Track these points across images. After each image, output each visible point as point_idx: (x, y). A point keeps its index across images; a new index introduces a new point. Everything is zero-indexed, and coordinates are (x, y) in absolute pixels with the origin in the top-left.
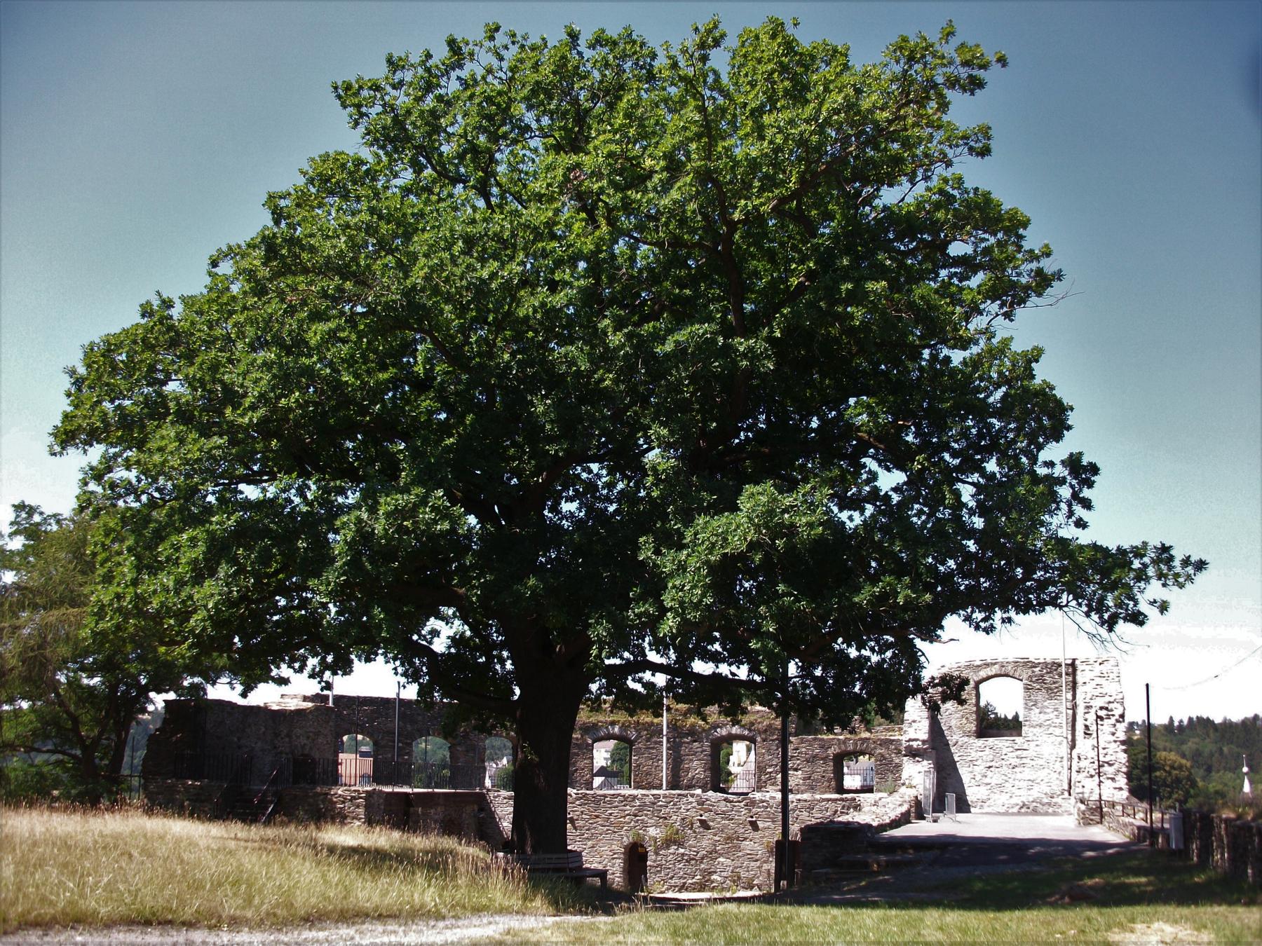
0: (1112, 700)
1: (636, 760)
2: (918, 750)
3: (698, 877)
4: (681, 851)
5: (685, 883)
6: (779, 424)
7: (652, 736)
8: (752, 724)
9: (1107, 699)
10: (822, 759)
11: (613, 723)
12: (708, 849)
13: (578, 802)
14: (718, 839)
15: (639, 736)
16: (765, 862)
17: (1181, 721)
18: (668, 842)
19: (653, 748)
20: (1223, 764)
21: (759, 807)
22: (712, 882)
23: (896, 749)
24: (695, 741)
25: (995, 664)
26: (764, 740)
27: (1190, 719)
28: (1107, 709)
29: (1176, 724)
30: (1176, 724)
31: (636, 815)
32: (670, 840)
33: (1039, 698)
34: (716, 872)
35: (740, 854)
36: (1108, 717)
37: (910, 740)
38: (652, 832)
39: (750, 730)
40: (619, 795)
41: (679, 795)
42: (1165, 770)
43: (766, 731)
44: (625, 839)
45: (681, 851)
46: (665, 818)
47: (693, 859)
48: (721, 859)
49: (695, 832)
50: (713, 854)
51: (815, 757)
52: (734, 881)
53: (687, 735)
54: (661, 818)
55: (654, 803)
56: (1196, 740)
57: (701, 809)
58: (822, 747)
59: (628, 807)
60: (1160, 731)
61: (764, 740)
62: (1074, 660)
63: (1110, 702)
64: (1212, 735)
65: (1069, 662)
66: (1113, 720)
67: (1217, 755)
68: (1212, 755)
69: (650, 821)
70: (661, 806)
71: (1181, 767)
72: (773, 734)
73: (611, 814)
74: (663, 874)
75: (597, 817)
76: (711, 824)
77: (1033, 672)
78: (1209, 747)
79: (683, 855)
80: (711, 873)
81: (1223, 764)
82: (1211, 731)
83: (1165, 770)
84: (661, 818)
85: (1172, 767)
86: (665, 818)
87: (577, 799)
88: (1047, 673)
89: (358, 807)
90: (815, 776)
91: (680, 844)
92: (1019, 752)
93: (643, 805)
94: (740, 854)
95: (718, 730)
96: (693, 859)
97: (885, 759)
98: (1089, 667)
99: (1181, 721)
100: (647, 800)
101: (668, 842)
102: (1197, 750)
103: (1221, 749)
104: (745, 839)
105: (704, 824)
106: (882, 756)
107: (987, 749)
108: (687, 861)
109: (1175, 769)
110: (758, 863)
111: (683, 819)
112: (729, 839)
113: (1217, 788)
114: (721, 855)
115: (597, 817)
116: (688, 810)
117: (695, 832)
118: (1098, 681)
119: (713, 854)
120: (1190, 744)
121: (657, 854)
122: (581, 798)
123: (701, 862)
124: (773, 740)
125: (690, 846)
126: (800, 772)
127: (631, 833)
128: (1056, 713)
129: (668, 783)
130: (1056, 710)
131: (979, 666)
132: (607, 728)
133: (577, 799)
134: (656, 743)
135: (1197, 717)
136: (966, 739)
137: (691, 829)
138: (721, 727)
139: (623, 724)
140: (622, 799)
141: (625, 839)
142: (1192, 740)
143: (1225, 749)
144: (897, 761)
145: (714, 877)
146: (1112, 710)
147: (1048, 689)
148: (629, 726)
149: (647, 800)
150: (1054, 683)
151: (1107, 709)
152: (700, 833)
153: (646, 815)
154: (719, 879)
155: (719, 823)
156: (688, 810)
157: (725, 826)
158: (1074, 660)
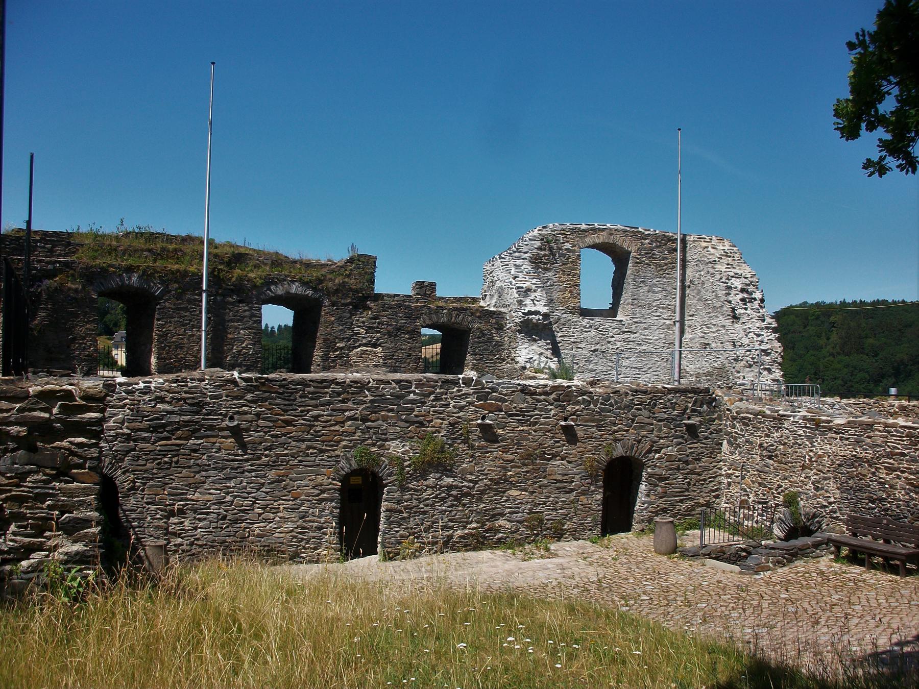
1: (162, 326)
2: (536, 325)
3: (474, 525)
4: (448, 481)
5: (451, 537)
7: (184, 291)
8: (320, 281)
10: (408, 332)
11: (130, 270)
12: (493, 476)
13: (249, 396)
14: (510, 457)
15: (166, 291)
16: (584, 493)
17: (273, 327)
18: (424, 468)
19: (186, 309)
21: (578, 403)
22: (497, 531)
23: (497, 323)
24: (240, 302)
25: (603, 230)
26: (333, 304)
31: (365, 420)
32: (430, 464)
33: (649, 274)
34: (502, 515)
35: (545, 481)
37: (530, 313)
38: (396, 448)
39: (315, 289)
40: (333, 381)
41: (446, 381)
43: (337, 291)
44: (343, 463)
45: (448, 481)
46: (421, 424)
47: (467, 495)
48: (514, 493)
49: (471, 447)
50: (500, 484)
51: (399, 329)
52: (532, 528)
53: (232, 292)
54: (413, 423)
55: (400, 397)
57: (481, 407)
58: (408, 317)
59: (350, 404)
61: (333, 304)
69: (391, 430)
70: (413, 402)
72: (347, 296)
73: (316, 418)
74: (412, 524)
75: (288, 423)
76: (500, 431)
77: (642, 244)
79: (450, 487)
80: (494, 517)
84: (413, 423)
86: (421, 424)
87: (248, 390)
88: (657, 247)
89: (63, 472)
90: (400, 355)
91: (446, 469)
92: (626, 336)
93: (379, 400)
94: (545, 481)
95: (272, 287)
96: (467, 495)
97: (484, 335)
99: (273, 327)
100: (387, 391)
101: (424, 468)
104: (554, 456)
105: (488, 433)
106: (481, 331)
107: (592, 329)
108: (456, 498)
110: (572, 496)
111: (452, 425)
112: (529, 457)
114: (513, 485)
115: (288, 423)
116: (461, 409)
117: (471, 447)
119: (500, 484)
121: (403, 488)
122: (256, 388)
123: (480, 500)
124: (345, 305)
125: (464, 471)
126: (379, 349)
127: (354, 452)
128: (664, 293)
129: (207, 359)
130: (664, 289)
131: (585, 231)
132: (120, 276)
133: (248, 390)
134: (189, 301)
135: (285, 325)
136: (569, 316)
137: (464, 442)
138: (276, 284)
139: (144, 272)
140: (338, 388)
141: (343, 463)
144: (498, 339)
145: (502, 522)
147: (657, 265)
148: (152, 275)
149: (387, 391)
150: (664, 259)
152: (480, 448)
153: (385, 419)
154: (508, 525)
155: (513, 430)
156: (461, 409)
157: (523, 436)
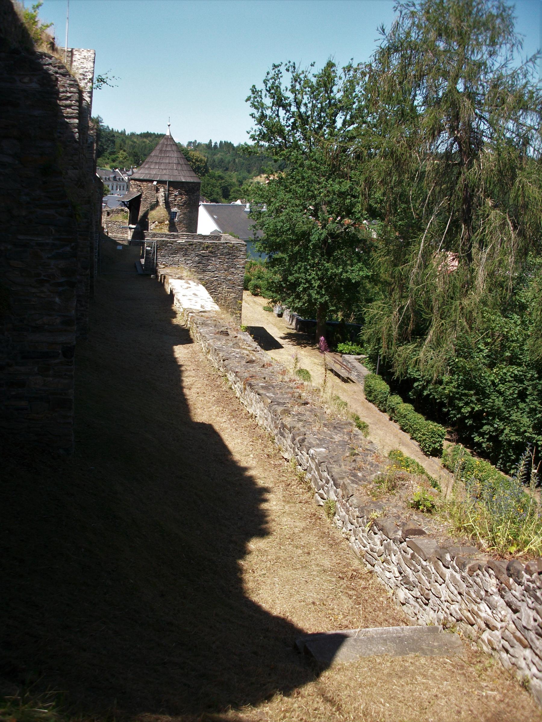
0: (87, 70)
6: (478, 8)
9: (85, 70)
20: (234, 168)
27: (221, 142)
28: (84, 75)
29: (213, 144)
30: (213, 144)
36: (84, 79)
42: (193, 162)
56: (223, 154)
60: (203, 147)
62: (72, 49)
63: (86, 72)
64: (231, 152)
65: (70, 50)
66: (86, 81)
67: (232, 163)
68: (229, 162)
71: (201, 161)
78: (228, 158)
81: (234, 168)
82: (231, 150)
83: (193, 162)
85: (197, 160)
98: (79, 53)
99: (216, 143)
102: (222, 159)
103: (234, 159)
109: (198, 162)
113: (220, 174)
118: (82, 60)
120: (218, 155)
142: (220, 153)
143: (237, 160)
146: (86, 76)
151: (84, 75)
158: (72, 49)
